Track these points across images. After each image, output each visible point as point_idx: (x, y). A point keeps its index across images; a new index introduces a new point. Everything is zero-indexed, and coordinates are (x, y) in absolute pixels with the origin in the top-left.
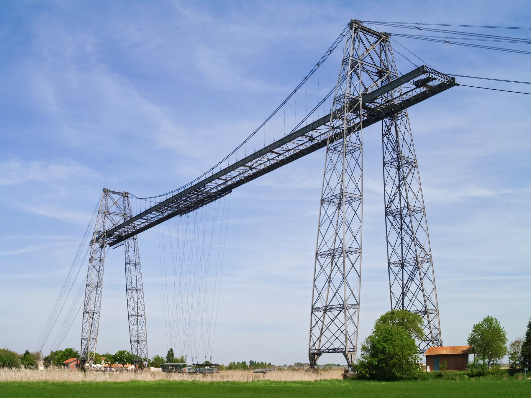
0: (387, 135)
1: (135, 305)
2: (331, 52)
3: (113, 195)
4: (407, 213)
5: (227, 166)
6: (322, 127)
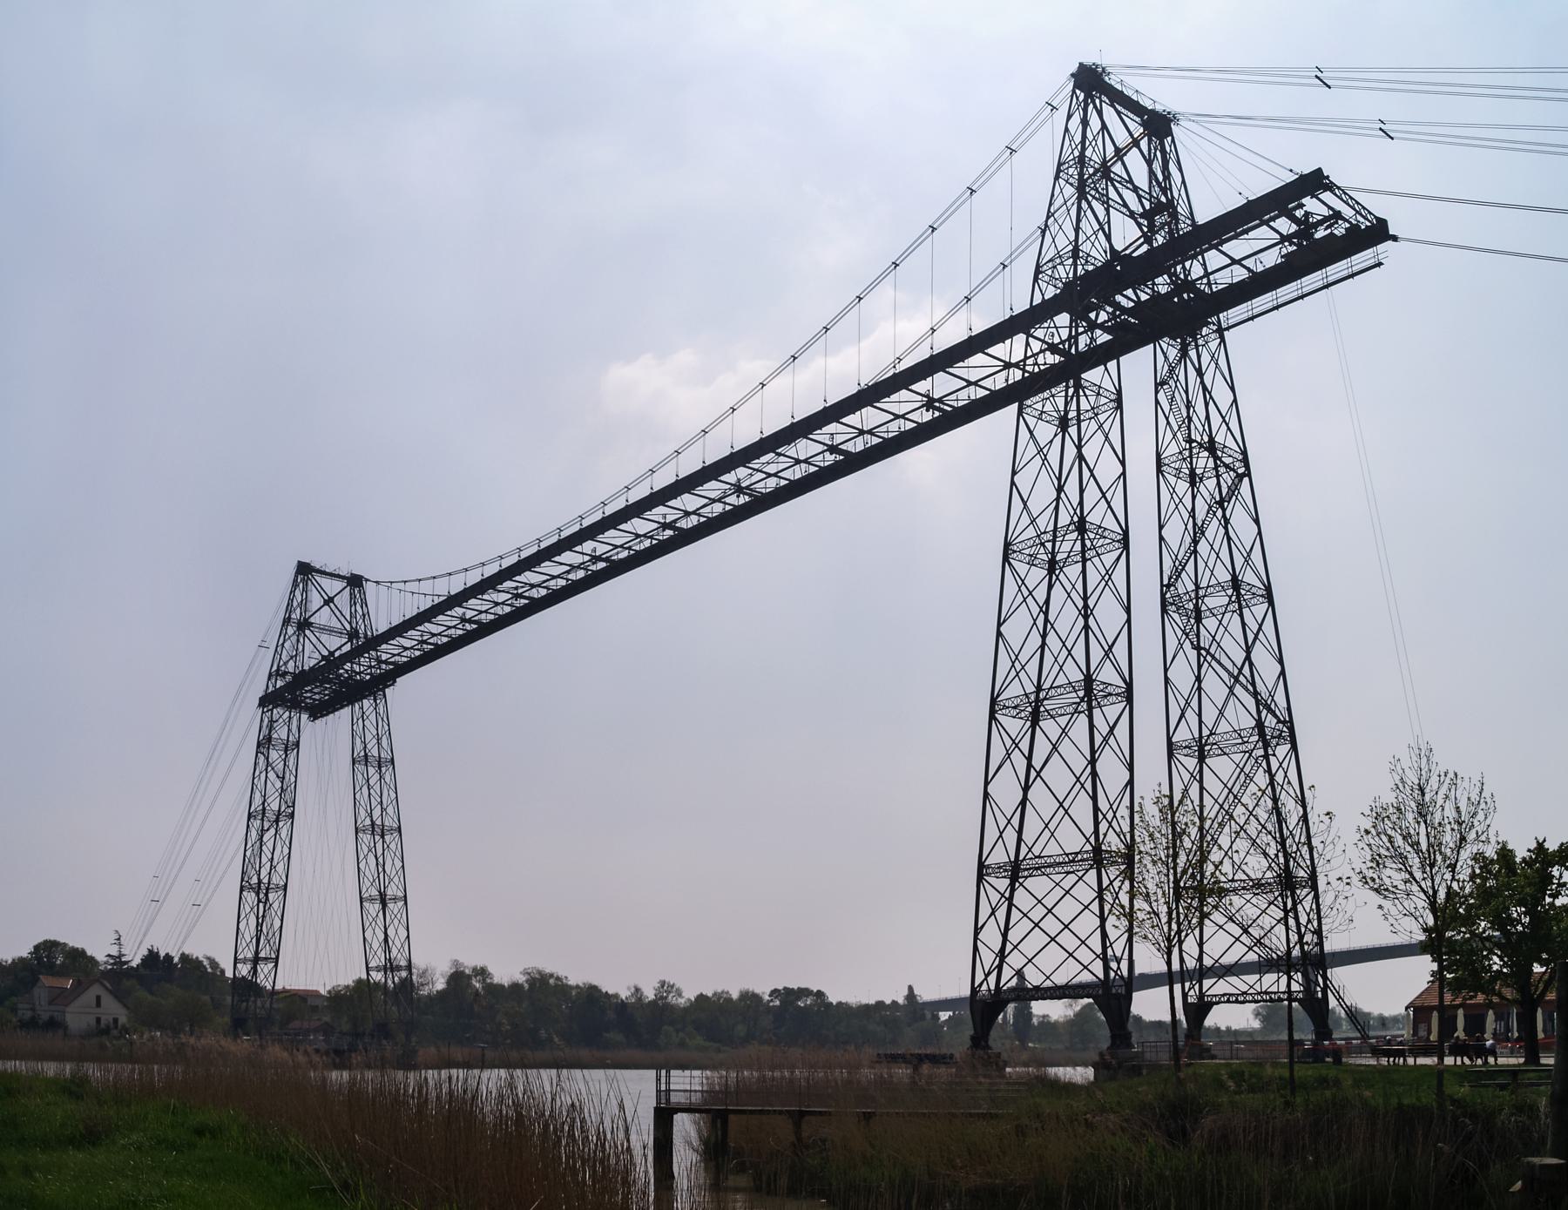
0: (1165, 387)
2: (1011, 153)
5: (647, 493)
6: (713, 484)
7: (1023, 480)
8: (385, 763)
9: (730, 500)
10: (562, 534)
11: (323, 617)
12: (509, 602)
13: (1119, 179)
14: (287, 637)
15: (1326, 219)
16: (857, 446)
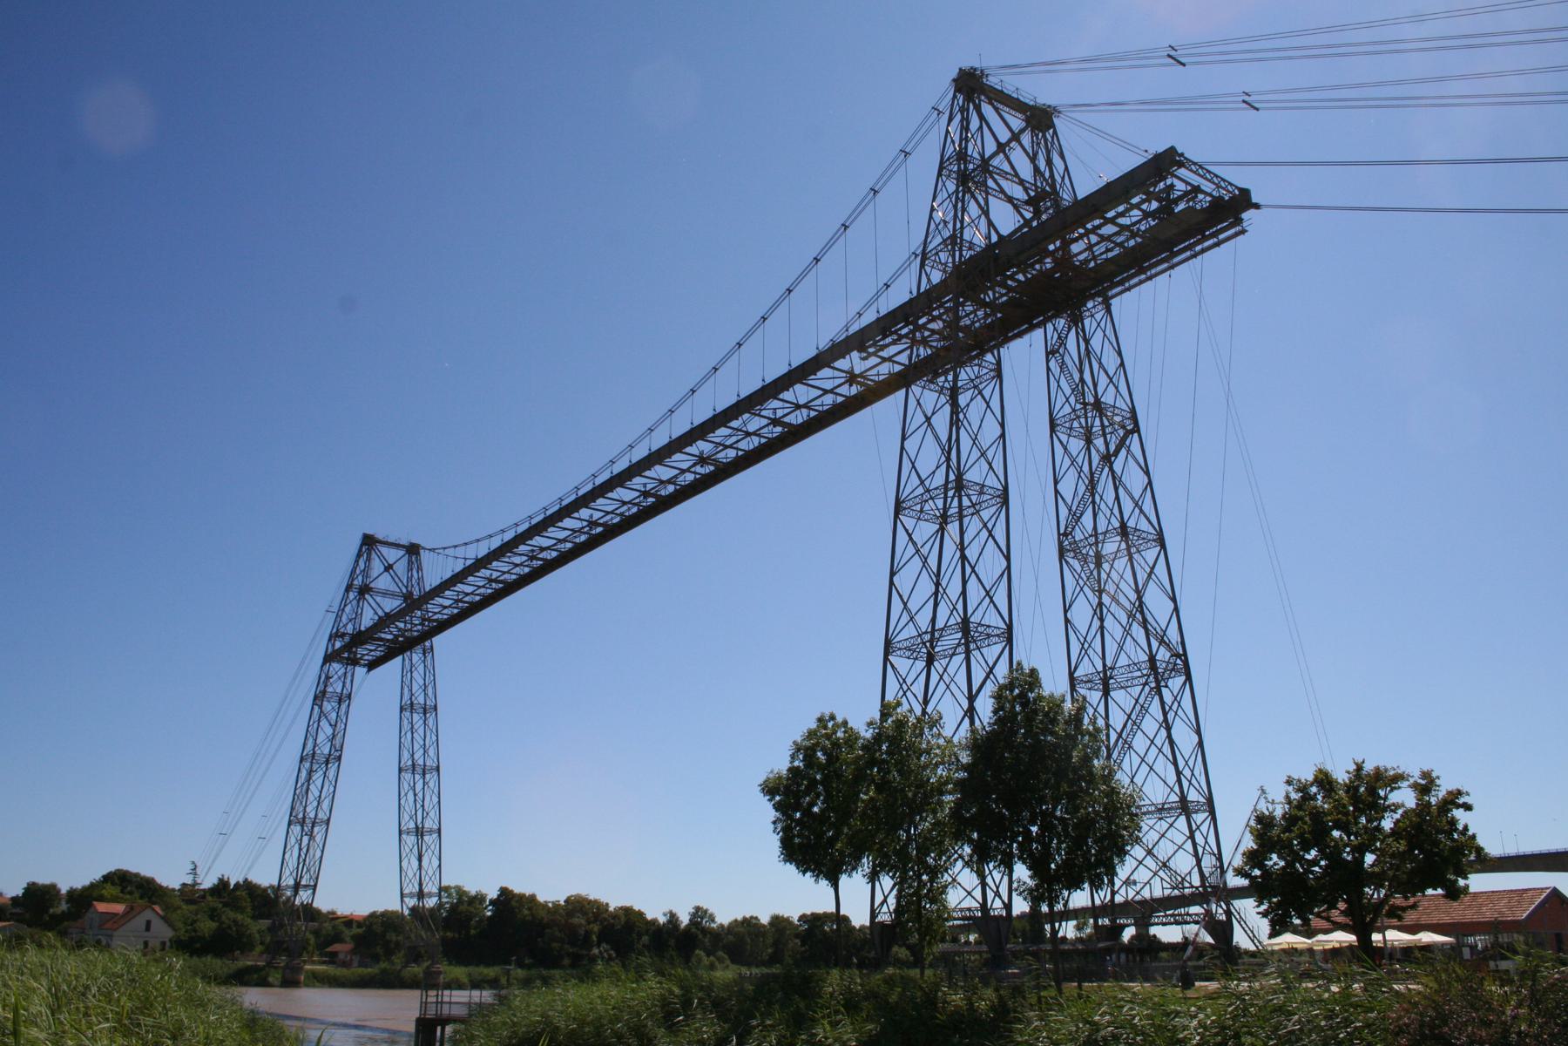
1: (418, 806)
3: (384, 550)
4: (1118, 551)
7: (903, 581)
8: (429, 710)
9: (841, 390)
10: (596, 479)
11: (384, 582)
12: (526, 563)
13: (998, 171)
14: (348, 601)
15: (1186, 193)
16: (797, 418)
